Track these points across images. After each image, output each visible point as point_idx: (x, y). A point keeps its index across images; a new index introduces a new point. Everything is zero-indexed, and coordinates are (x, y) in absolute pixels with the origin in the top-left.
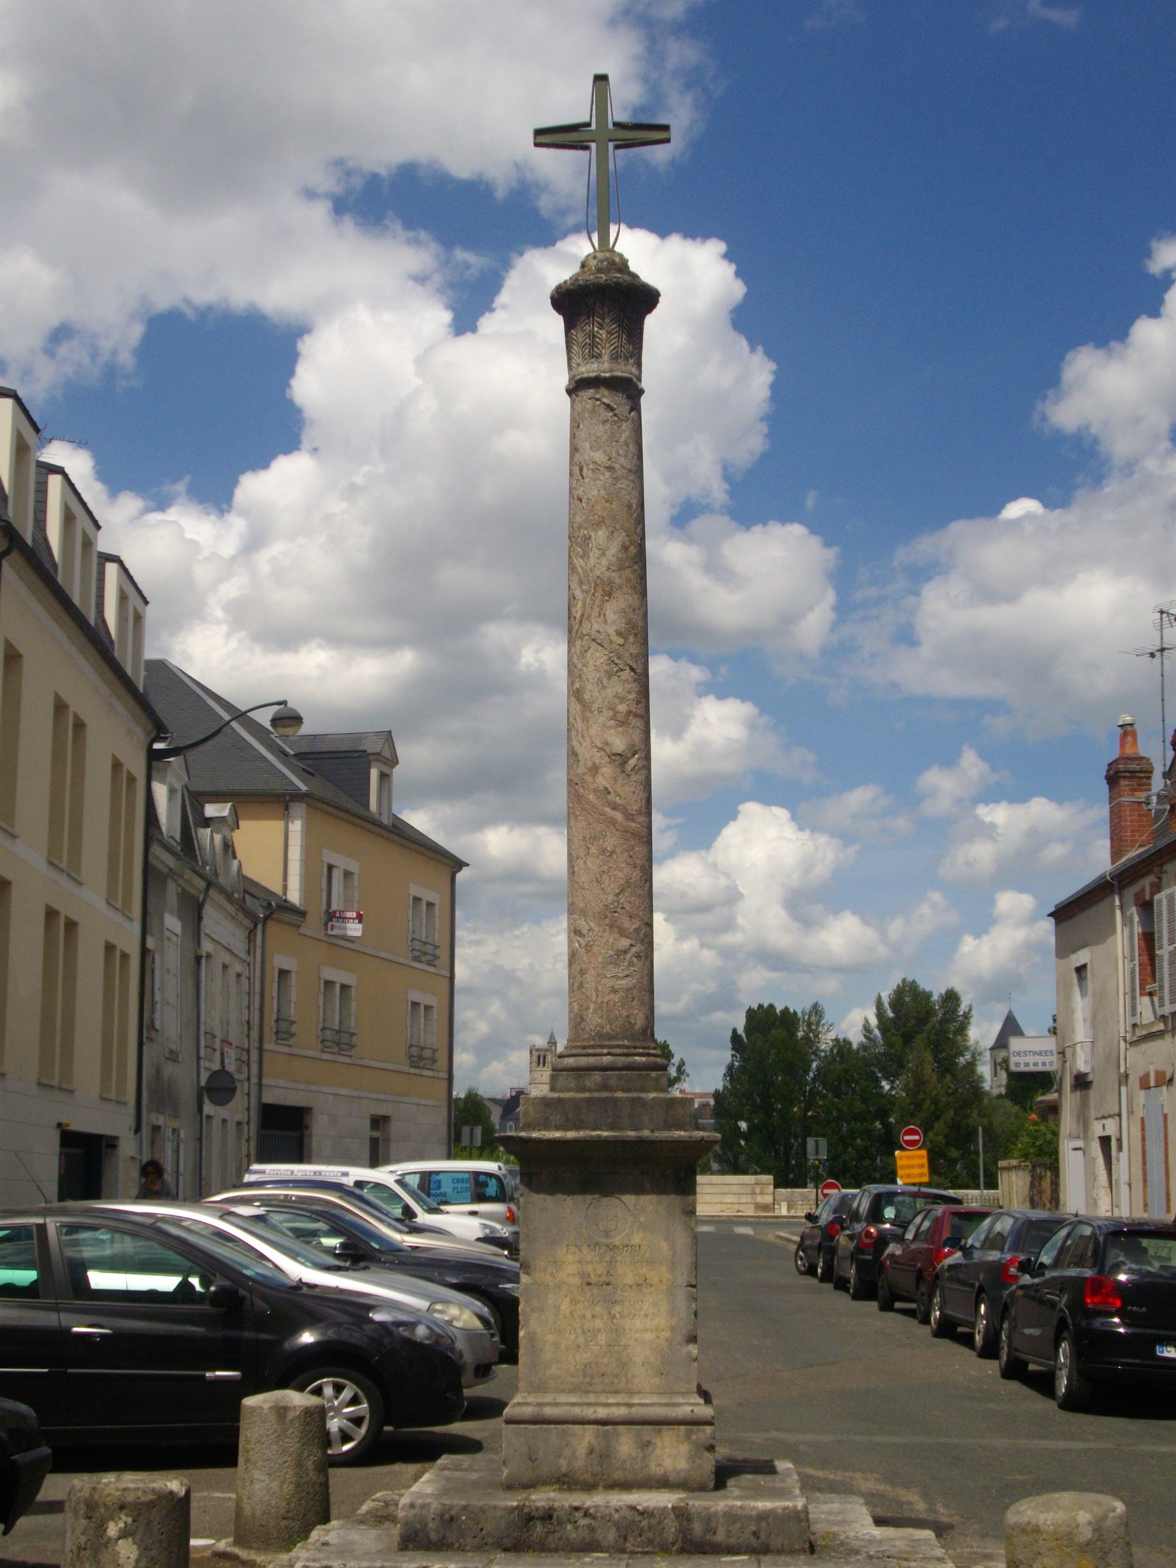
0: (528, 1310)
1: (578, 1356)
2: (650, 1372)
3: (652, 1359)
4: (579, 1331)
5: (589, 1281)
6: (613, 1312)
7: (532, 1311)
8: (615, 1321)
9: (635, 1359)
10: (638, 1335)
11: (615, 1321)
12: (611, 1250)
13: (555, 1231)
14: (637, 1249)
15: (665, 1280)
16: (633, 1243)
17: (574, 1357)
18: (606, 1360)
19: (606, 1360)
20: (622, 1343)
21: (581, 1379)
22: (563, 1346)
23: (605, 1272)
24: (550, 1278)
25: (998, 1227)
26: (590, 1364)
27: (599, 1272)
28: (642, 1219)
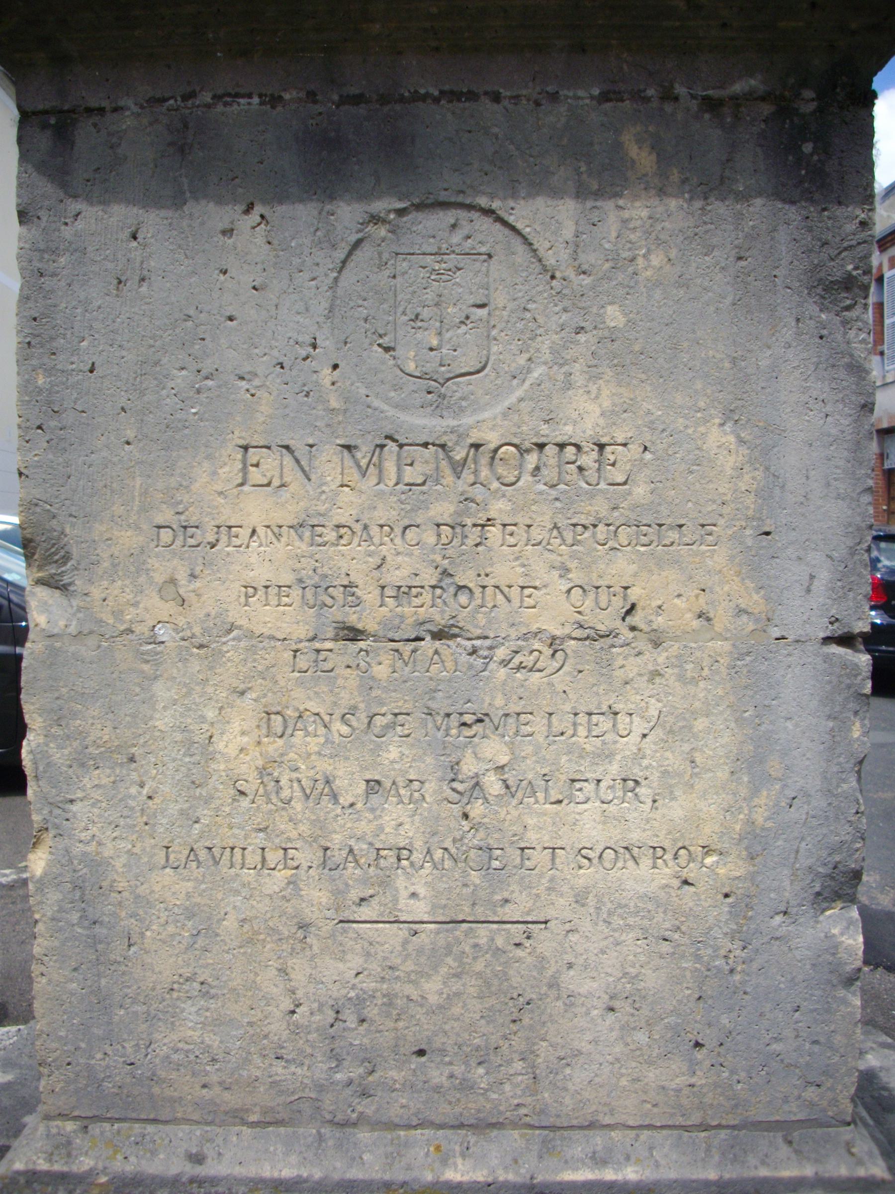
0: (59, 756)
1: (300, 969)
2: (641, 1037)
3: (652, 980)
4: (304, 856)
5: (353, 619)
6: (469, 767)
7: (82, 762)
8: (477, 809)
9: (571, 981)
10: (587, 875)
11: (477, 809)
12: (458, 468)
13: (181, 379)
14: (588, 459)
15: (722, 618)
16: (566, 432)
17: (283, 971)
18: (433, 988)
19: (433, 988)
20: (510, 912)
21: (321, 1068)
22: (230, 923)
23: (429, 577)
24: (166, 609)
25: (56, 644)
26: (359, 1002)
27: (396, 576)
28: (614, 316)
